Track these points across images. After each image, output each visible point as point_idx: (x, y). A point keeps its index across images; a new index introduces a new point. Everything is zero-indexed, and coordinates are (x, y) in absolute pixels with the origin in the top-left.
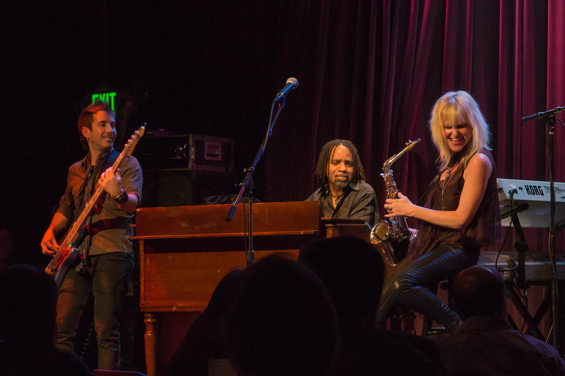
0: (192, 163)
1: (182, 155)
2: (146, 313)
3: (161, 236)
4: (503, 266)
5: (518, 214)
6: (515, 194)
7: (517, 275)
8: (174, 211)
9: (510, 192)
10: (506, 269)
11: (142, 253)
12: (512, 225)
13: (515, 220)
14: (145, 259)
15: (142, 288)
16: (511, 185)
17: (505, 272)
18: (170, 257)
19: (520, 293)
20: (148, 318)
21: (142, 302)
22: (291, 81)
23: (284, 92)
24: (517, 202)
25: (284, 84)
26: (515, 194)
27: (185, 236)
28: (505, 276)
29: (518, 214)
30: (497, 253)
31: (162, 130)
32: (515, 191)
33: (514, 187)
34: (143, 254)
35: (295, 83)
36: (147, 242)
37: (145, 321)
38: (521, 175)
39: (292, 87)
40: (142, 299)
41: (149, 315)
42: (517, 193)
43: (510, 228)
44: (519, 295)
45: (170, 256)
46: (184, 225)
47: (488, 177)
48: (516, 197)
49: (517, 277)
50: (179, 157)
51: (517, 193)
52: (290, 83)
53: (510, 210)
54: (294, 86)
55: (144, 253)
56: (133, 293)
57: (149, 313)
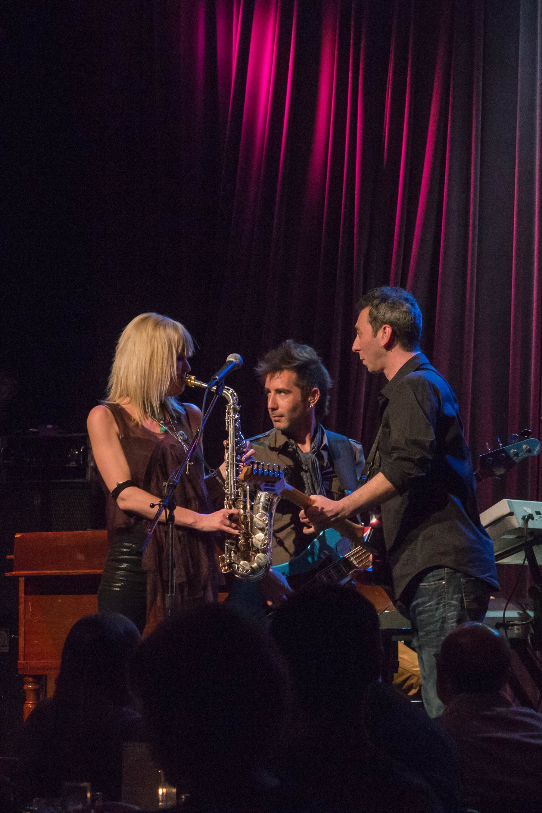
0: (418, 336)
1: (78, 462)
2: (25, 676)
3: (49, 572)
4: (512, 619)
5: (535, 548)
6: (530, 521)
7: (532, 631)
8: (64, 537)
9: (523, 518)
10: (516, 622)
11: (22, 595)
12: (526, 563)
13: (531, 557)
14: (26, 602)
15: (21, 642)
16: (525, 508)
17: (516, 627)
18: (60, 601)
19: (535, 656)
20: (29, 683)
21: (21, 661)
22: (233, 358)
23: (221, 376)
24: (533, 532)
25: (223, 362)
26: (530, 521)
27: (81, 572)
28: (516, 632)
29: (535, 548)
30: (506, 601)
31: (50, 426)
32: (531, 517)
33: (529, 511)
34: (23, 595)
35: (238, 361)
36: (28, 579)
37: (25, 687)
38: (537, 496)
39: (233, 368)
40: (21, 657)
41: (31, 679)
42: (533, 519)
43: (523, 566)
44: (534, 658)
45: (60, 599)
46: (80, 557)
47: (125, 418)
48: (531, 524)
49: (531, 634)
50: (73, 464)
51: (533, 519)
52: (231, 362)
53: (524, 542)
54: (236, 365)
55: (25, 594)
56: (8, 648)
57: (29, 676)
